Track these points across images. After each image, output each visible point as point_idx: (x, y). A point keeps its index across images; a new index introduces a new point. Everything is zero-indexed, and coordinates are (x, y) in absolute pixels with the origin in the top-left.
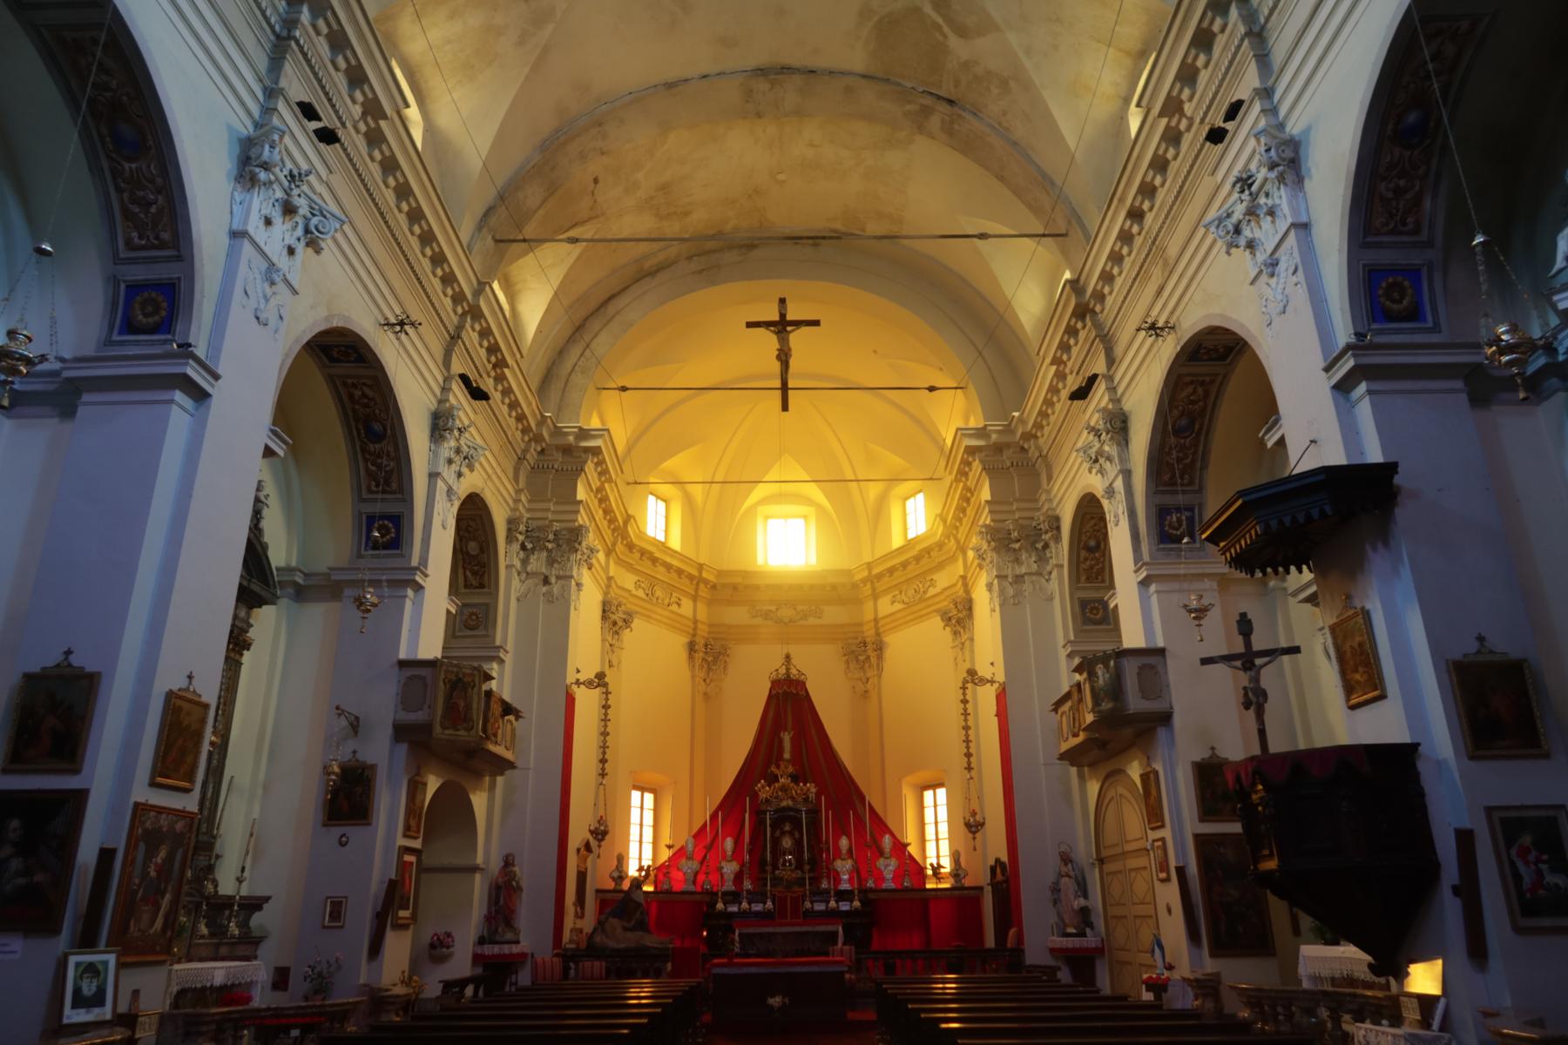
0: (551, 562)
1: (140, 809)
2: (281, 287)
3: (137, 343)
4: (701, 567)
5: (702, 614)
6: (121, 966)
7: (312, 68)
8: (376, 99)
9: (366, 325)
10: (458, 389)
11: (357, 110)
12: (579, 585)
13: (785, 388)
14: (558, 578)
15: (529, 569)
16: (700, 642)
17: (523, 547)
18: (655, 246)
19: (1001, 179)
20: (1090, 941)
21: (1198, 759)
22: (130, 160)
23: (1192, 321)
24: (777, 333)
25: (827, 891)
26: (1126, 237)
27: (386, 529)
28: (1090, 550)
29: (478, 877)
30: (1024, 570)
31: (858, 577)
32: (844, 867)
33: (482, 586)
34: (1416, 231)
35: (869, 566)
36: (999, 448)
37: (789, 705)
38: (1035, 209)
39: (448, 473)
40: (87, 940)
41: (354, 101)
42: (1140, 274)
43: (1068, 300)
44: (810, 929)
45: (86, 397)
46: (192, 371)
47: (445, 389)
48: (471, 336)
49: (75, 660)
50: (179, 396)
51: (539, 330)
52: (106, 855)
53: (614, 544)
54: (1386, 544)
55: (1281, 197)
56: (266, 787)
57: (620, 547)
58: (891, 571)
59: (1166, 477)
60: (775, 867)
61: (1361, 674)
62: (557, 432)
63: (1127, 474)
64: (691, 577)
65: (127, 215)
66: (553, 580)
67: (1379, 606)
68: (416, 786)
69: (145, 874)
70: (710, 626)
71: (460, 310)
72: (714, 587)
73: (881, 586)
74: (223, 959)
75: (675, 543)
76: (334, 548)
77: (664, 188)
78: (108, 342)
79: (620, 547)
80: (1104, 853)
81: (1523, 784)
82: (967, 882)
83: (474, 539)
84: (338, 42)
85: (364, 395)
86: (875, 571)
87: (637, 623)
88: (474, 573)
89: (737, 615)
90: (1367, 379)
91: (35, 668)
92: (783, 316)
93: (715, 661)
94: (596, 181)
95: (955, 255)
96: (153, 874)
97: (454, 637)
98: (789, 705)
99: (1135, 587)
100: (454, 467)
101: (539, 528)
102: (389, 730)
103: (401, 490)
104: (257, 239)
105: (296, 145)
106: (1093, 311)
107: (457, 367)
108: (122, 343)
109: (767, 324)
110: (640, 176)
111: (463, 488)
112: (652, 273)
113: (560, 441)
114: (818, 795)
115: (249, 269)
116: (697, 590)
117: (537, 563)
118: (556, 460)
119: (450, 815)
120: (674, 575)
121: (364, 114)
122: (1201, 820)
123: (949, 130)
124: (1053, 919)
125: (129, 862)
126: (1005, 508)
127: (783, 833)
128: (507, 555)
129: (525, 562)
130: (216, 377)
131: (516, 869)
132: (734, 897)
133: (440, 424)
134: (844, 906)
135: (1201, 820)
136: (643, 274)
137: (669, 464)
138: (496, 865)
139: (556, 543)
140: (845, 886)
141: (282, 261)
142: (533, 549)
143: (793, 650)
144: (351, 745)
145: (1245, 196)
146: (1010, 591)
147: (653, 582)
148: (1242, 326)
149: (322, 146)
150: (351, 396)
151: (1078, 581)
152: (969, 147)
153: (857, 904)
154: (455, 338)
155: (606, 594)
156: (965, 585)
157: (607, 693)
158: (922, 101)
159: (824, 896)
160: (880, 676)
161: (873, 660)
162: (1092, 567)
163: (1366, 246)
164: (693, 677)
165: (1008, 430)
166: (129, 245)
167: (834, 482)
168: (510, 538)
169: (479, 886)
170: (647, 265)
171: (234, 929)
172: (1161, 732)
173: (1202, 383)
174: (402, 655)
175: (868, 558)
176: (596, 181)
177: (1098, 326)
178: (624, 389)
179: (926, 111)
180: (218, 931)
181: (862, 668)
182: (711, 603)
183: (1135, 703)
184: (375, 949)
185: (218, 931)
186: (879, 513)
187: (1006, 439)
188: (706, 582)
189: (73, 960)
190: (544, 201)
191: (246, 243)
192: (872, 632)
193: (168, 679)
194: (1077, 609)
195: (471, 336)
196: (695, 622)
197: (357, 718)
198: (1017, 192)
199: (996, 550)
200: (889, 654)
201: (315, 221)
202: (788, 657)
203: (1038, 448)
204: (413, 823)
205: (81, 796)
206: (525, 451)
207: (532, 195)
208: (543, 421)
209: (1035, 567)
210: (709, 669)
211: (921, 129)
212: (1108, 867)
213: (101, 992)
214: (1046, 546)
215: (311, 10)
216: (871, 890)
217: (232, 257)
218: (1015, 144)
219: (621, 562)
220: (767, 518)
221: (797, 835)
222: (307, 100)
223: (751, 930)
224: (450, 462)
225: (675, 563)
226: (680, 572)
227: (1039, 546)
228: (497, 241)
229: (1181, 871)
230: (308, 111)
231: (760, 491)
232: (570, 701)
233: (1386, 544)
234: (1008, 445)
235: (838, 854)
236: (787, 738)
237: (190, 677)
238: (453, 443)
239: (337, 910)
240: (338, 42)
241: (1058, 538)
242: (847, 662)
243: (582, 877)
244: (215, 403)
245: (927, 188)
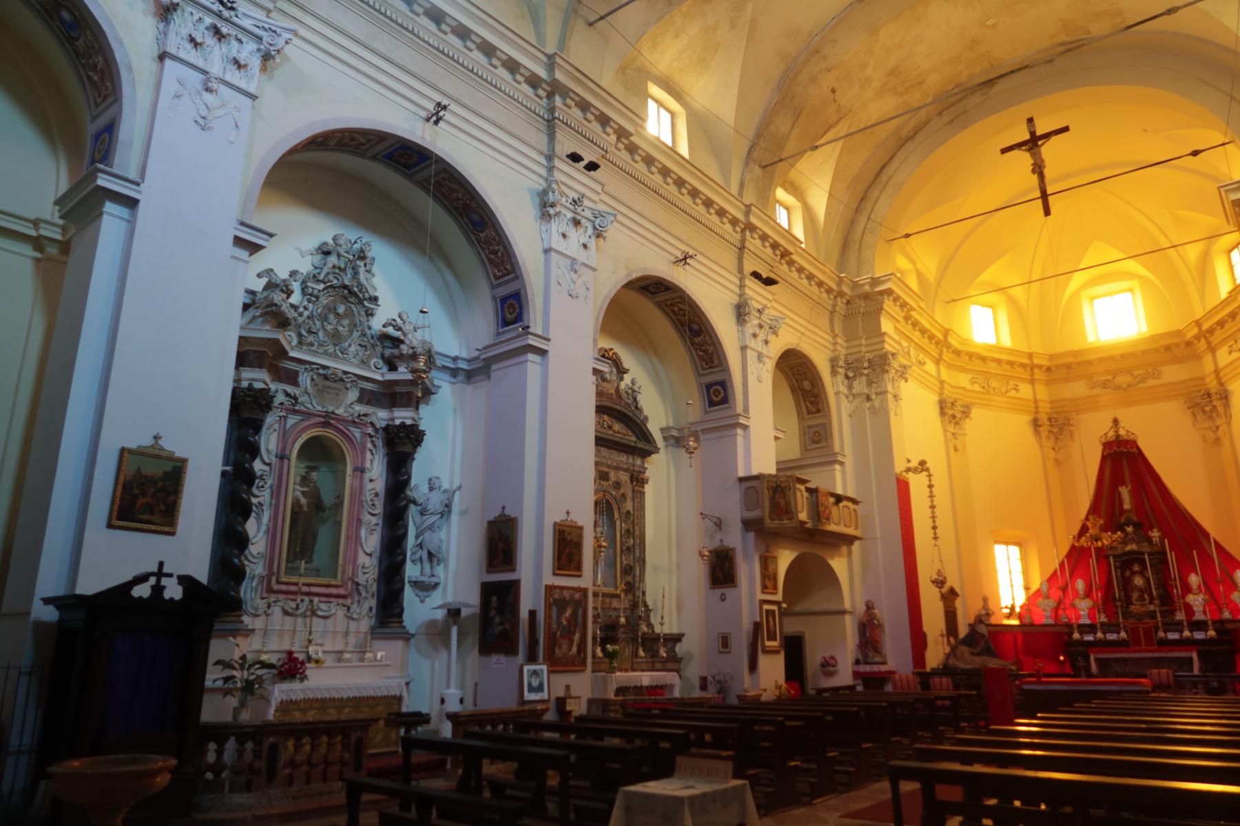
0: (870, 383)
1: (550, 589)
2: (583, 270)
3: (509, 331)
4: (1030, 355)
6: (550, 672)
7: (574, 129)
8: (621, 127)
9: (660, 267)
10: (752, 284)
11: (613, 138)
12: (895, 397)
13: (1044, 196)
14: (877, 394)
15: (854, 391)
16: (1043, 418)
17: (847, 377)
18: (906, 117)
22: (482, 232)
24: (1029, 150)
25: (1180, 623)
27: (718, 394)
29: (848, 618)
31: (1190, 335)
32: (1197, 601)
33: (819, 411)
35: (1198, 323)
37: (1124, 462)
39: (756, 344)
40: (532, 658)
41: (608, 135)
44: (1163, 655)
45: (494, 367)
46: (532, 341)
47: (742, 286)
48: (754, 243)
49: (507, 512)
50: (530, 356)
51: (828, 213)
52: (532, 614)
53: (940, 355)
56: (678, 566)
57: (947, 356)
58: (1221, 323)
60: (1128, 601)
62: (855, 285)
64: (1024, 366)
65: (491, 261)
66: (873, 397)
68: (767, 563)
69: (559, 623)
70: (1051, 402)
71: (738, 229)
72: (1049, 369)
73: (1215, 339)
74: (658, 670)
75: (1007, 341)
76: (694, 408)
77: (893, 72)
78: (498, 334)
79: (947, 356)
83: (806, 379)
84: (584, 106)
85: (680, 309)
86: (1205, 327)
87: (975, 412)
88: (812, 403)
91: (491, 518)
92: (1033, 133)
93: (1061, 430)
94: (833, 91)
95: (1183, 23)
96: (565, 623)
97: (806, 450)
98: (1124, 462)
100: (759, 339)
101: (858, 360)
102: (739, 525)
103: (721, 364)
104: (560, 249)
105: (572, 179)
107: (749, 267)
108: (503, 333)
109: (1019, 146)
110: (869, 71)
111: (775, 349)
112: (910, 138)
113: (859, 292)
114: (1161, 539)
115: (559, 268)
116: (1032, 375)
117: (860, 386)
118: (859, 307)
119: (810, 577)
120: (1007, 367)
121: (619, 139)
125: (548, 616)
127: (1134, 573)
128: (833, 386)
129: (850, 387)
130: (549, 340)
131: (876, 611)
133: (741, 312)
134: (1199, 635)
136: (902, 142)
137: (985, 276)
138: (861, 608)
139: (870, 368)
140: (1199, 616)
141: (582, 256)
142: (855, 376)
143: (1121, 414)
144: (718, 536)
147: (987, 376)
149: (592, 173)
150: (673, 312)
153: (1212, 633)
154: (742, 248)
155: (941, 394)
157: (930, 476)
159: (1178, 627)
160: (1229, 423)
161: (1221, 409)
164: (1042, 447)
166: (497, 278)
167: (1150, 253)
168: (834, 373)
169: (850, 626)
170: (904, 133)
171: (663, 653)
174: (741, 474)
175: (1199, 314)
176: (833, 91)
178: (907, 236)
180: (654, 654)
181: (1211, 418)
182: (1049, 383)
184: (753, 666)
185: (654, 654)
186: (1204, 267)
188: (1040, 367)
189: (526, 668)
190: (794, 124)
191: (553, 254)
192: (1215, 383)
193: (554, 515)
195: (754, 243)
196: (1036, 401)
197: (719, 519)
201: (597, 221)
202: (1116, 421)
204: (769, 584)
205: (515, 585)
206: (834, 306)
207: (782, 124)
208: (840, 281)
210: (1057, 438)
213: (541, 685)
215: (561, 96)
216: (1228, 621)
217: (547, 264)
219: (950, 367)
220: (1092, 299)
222: (573, 150)
223: (1106, 656)
224: (755, 335)
225: (1003, 357)
226: (1011, 364)
228: (764, 167)
230: (575, 158)
231: (1078, 279)
232: (903, 488)
235: (1187, 589)
236: (1125, 492)
237: (568, 513)
238: (756, 322)
239: (725, 641)
240: (584, 106)
242: (1194, 415)
244: (551, 354)
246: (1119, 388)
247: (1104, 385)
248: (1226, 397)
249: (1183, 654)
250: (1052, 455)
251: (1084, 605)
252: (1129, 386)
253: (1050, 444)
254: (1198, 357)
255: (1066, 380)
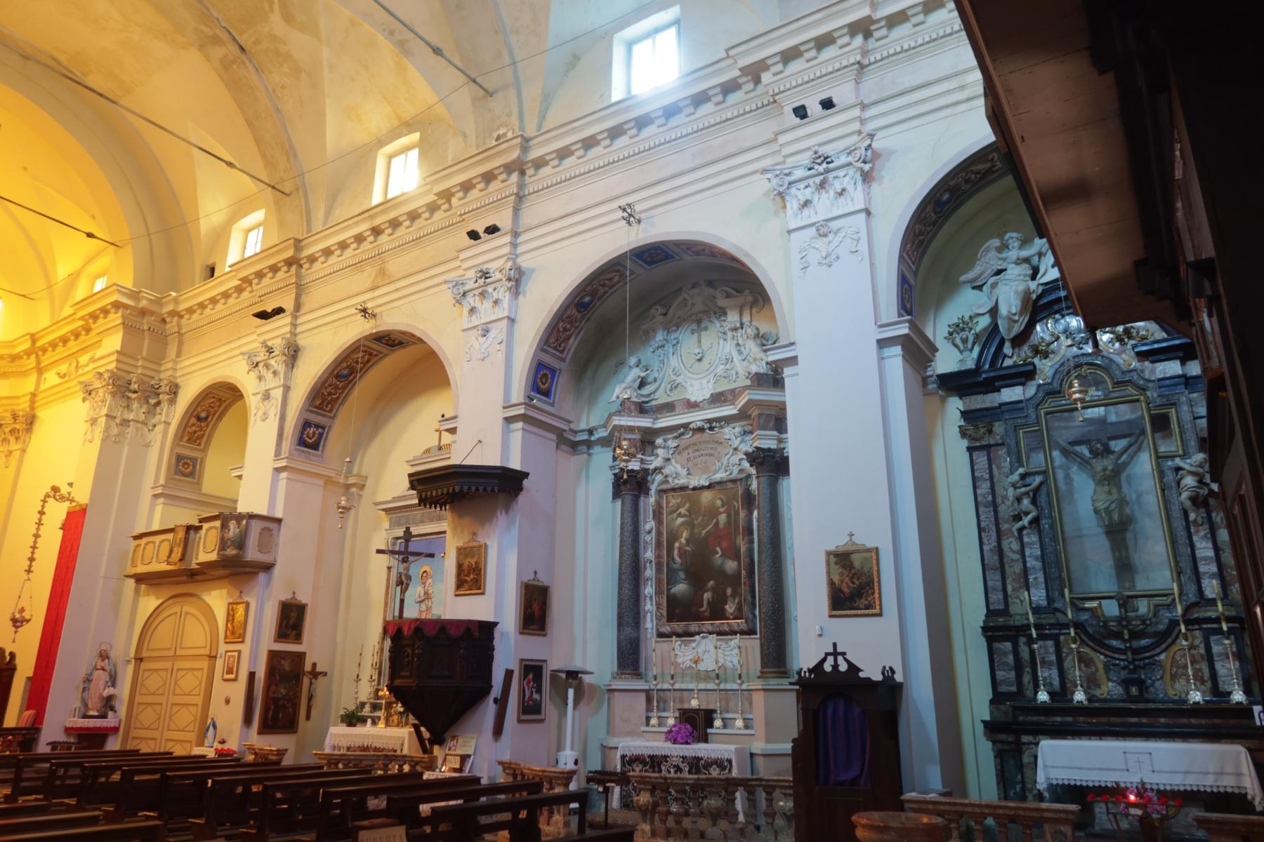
19: (250, 124)
20: (110, 721)
21: (283, 599)
23: (393, 320)
26: (360, 239)
28: (199, 419)
30: (131, 416)
34: (562, 352)
36: (143, 313)
38: (269, 163)
42: (357, 266)
43: (286, 249)
54: (507, 512)
55: (504, 296)
59: (318, 402)
61: (470, 578)
63: (287, 389)
67: (496, 545)
80: (144, 654)
81: (533, 648)
90: (524, 421)
99: (271, 471)
106: (301, 266)
122: (275, 641)
123: (226, 64)
124: (78, 704)
126: (132, 362)
135: (275, 641)
145: (481, 281)
146: (115, 430)
148: (440, 347)
151: (181, 439)
152: (235, 86)
156: (33, 402)
158: (218, 32)
162: (195, 432)
163: (543, 350)
165: (159, 302)
172: (262, 577)
173: (371, 354)
177: (298, 276)
179: (216, 40)
183: (252, 553)
187: (153, 308)
194: (173, 461)
198: (258, 141)
199: (113, 394)
203: (179, 325)
209: (142, 417)
211: (201, 47)
212: (144, 665)
214: (158, 403)
218: (278, 110)
227: (152, 401)
229: (252, 676)
233: (507, 512)
234: (152, 313)
241: (172, 401)
245: (175, 88)
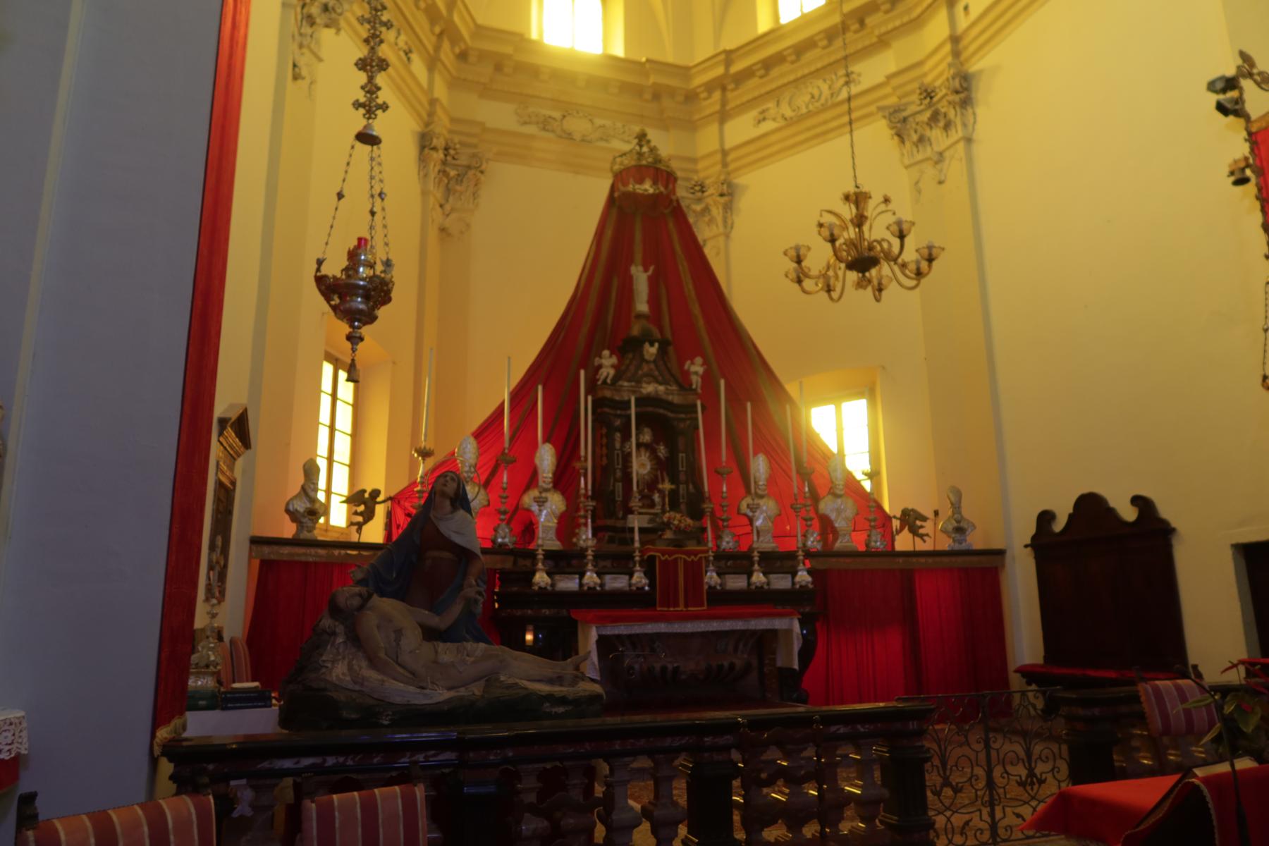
5: (440, 91)
35: (729, 56)
52: (450, 689)
73: (736, 97)
82: (976, 541)
89: (497, 115)
93: (460, 179)
132: (564, 561)
160: (727, 236)
161: (717, 212)
164: (424, 193)
182: (455, 83)
200: (745, 203)
210: (448, 191)
221: (662, 451)
223: (622, 629)
236: (641, 279)
243: (226, 494)
246: (569, 136)
247: (545, 124)
248: (731, 194)
249: (763, 624)
250: (437, 214)
251: (548, 510)
252: (583, 140)
253: (439, 194)
254: (691, 126)
255: (486, 91)
